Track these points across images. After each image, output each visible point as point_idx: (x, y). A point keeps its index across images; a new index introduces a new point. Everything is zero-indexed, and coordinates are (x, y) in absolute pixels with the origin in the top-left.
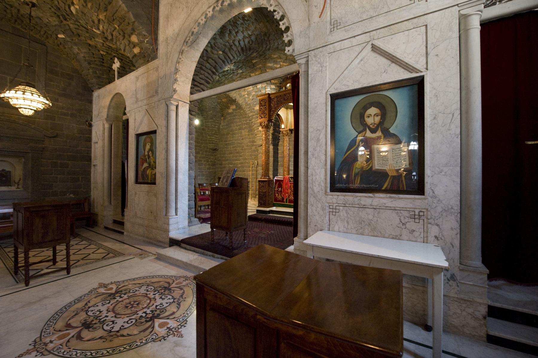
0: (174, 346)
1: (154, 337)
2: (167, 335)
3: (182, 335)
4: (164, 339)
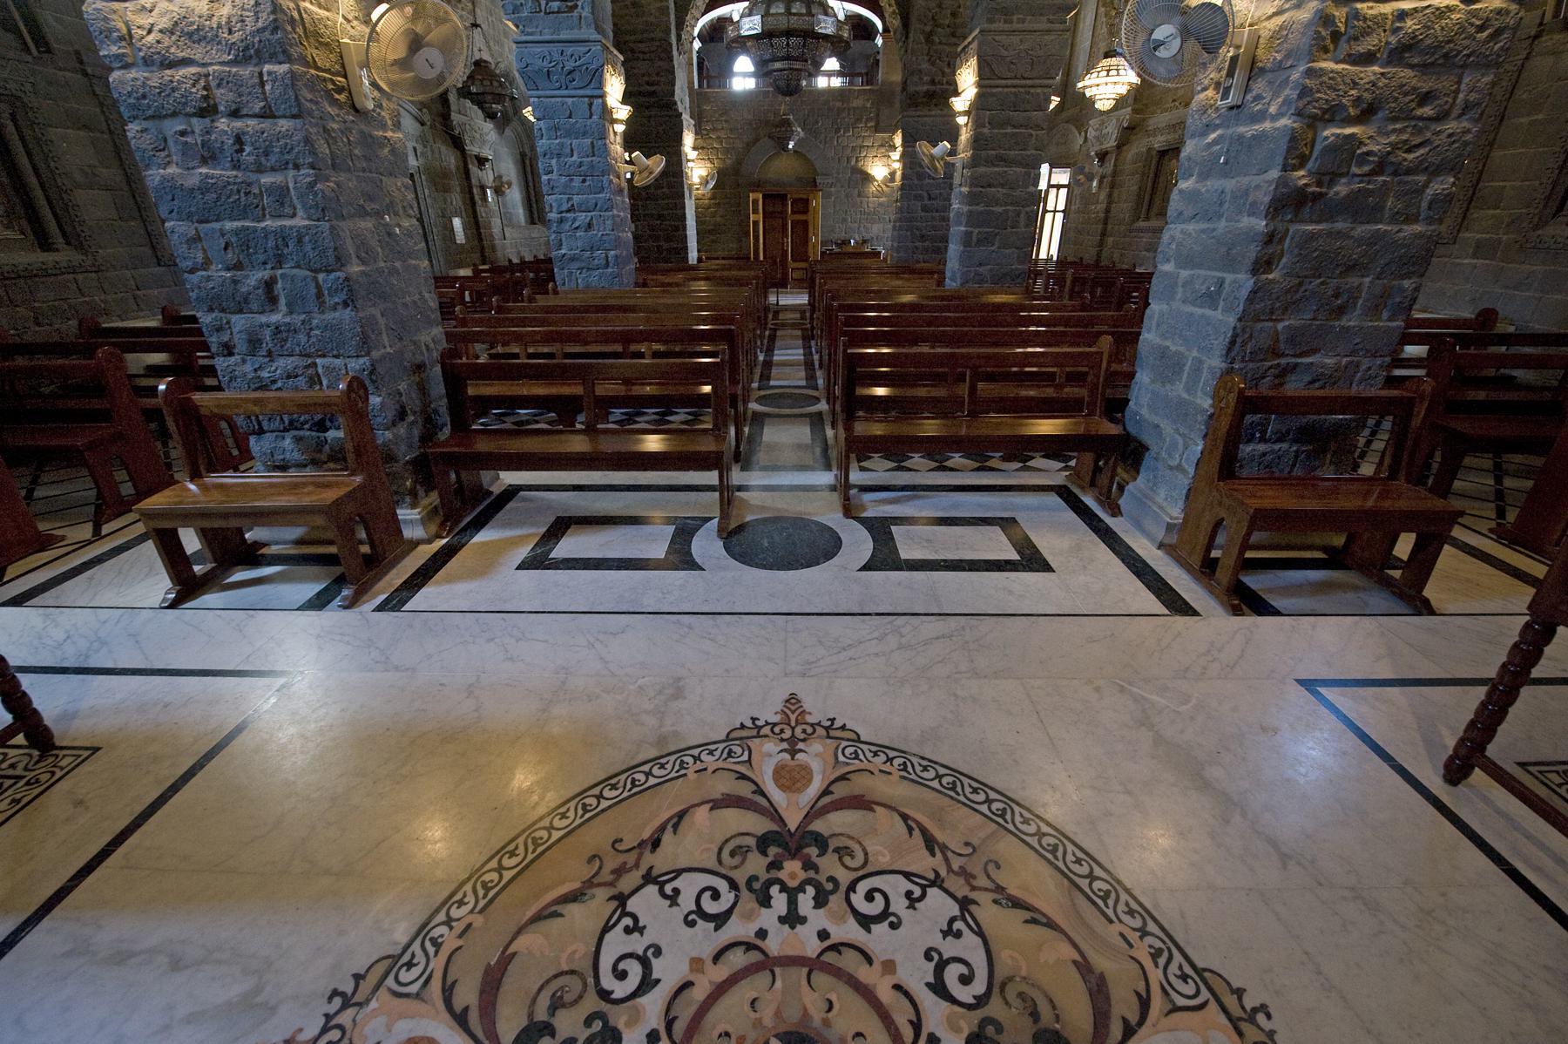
0: (258, 990)
1: (405, 976)
2: (340, 1027)
3: (787, 701)
4: (343, 994)
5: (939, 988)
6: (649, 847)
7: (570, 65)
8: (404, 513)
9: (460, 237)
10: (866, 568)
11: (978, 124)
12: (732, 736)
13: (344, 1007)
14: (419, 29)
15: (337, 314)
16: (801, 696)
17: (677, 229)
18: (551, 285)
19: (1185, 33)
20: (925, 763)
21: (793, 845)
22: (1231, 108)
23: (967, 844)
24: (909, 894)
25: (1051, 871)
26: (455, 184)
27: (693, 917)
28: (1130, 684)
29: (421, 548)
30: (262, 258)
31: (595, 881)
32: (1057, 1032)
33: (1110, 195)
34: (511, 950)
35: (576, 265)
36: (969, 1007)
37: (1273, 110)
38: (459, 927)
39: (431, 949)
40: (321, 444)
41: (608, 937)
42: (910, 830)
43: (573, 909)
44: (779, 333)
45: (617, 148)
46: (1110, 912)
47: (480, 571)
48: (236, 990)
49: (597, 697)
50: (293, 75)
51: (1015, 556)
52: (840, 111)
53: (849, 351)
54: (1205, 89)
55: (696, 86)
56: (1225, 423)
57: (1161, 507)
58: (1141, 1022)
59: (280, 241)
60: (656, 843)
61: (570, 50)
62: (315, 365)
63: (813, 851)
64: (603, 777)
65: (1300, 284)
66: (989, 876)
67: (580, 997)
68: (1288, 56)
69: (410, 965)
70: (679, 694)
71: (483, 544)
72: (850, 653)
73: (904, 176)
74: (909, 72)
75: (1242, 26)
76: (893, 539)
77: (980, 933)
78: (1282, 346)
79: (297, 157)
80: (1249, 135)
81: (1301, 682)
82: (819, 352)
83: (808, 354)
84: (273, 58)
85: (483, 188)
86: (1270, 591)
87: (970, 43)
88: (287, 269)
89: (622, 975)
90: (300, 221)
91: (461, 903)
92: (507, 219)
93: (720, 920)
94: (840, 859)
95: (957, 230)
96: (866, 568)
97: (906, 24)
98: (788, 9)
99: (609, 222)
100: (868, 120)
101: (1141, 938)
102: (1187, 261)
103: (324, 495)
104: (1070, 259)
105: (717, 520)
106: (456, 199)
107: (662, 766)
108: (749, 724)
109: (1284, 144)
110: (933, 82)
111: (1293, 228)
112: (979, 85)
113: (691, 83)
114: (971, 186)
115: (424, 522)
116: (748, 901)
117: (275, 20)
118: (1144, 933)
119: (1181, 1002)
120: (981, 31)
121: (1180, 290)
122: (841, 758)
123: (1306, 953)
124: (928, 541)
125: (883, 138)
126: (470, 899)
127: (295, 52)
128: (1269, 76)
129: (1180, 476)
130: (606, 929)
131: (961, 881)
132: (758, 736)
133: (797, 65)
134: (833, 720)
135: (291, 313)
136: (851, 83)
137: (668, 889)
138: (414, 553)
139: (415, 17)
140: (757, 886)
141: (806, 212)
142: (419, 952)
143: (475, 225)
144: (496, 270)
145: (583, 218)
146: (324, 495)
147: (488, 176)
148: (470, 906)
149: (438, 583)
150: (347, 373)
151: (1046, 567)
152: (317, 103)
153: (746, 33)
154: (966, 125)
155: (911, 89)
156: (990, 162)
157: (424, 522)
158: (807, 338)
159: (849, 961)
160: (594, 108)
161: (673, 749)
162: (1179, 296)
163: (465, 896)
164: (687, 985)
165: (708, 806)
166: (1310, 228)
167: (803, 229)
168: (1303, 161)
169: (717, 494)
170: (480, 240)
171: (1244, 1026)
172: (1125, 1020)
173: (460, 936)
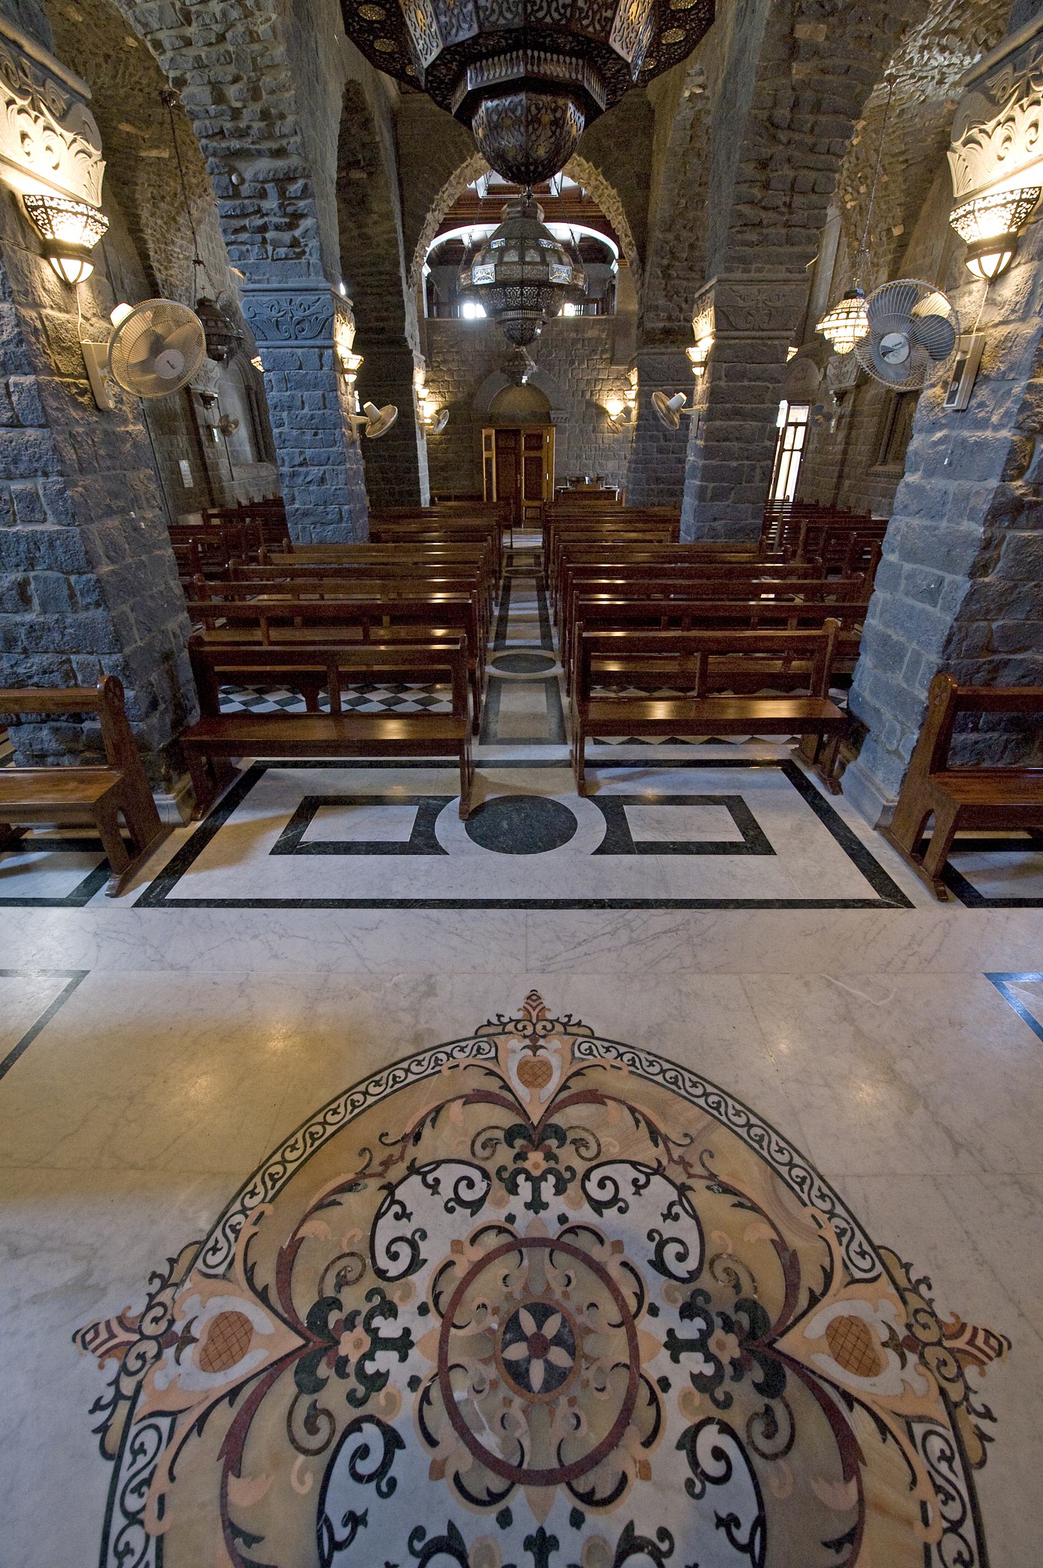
0: (89, 1273)
1: (212, 1260)
2: (162, 1304)
3: (529, 998)
5: (659, 1265)
6: (412, 1141)
7: (299, 315)
8: (161, 798)
9: (188, 482)
10: (600, 851)
11: (714, 377)
12: (480, 1033)
13: (163, 1288)
14: (159, 330)
15: (90, 613)
16: (540, 993)
17: (408, 471)
18: (285, 541)
19: (913, 341)
20: (651, 1058)
21: (535, 1137)
22: (957, 411)
23: (686, 1135)
24: (635, 1182)
25: (756, 1158)
26: (182, 425)
27: (452, 1204)
28: (837, 979)
29: (178, 831)
30: (14, 561)
31: (367, 1172)
32: (755, 1302)
33: (848, 436)
34: (299, 1236)
35: (307, 521)
36: (683, 1280)
37: (995, 419)
38: (253, 1215)
39: (231, 1236)
40: (77, 735)
41: (381, 1222)
42: (637, 1122)
43: (348, 1198)
44: (514, 582)
45: (351, 399)
46: (805, 1197)
47: (234, 857)
48: (71, 1273)
49: (358, 995)
50: (40, 387)
51: (739, 838)
52: (575, 341)
53: (585, 635)
54: (933, 386)
55: (426, 315)
56: (939, 718)
57: (879, 790)
58: (823, 1294)
59: (32, 545)
60: (417, 1137)
61: (298, 299)
62: (69, 661)
63: (553, 1143)
64: (368, 1074)
65: (1016, 586)
66: (703, 1165)
67: (361, 1276)
68: (1010, 369)
69: (215, 1250)
70: (431, 991)
71: (238, 827)
72: (584, 948)
73: (640, 417)
74: (647, 307)
75: (968, 332)
76: (625, 819)
77: (695, 1217)
78: (996, 644)
79: (46, 465)
80: (972, 440)
81: (988, 975)
82: (554, 605)
83: (543, 608)
84: (18, 369)
85: (209, 428)
86: (977, 874)
87: (707, 291)
88: (38, 572)
89: (394, 1257)
90: (51, 526)
91: (253, 1194)
92: (235, 460)
93: (475, 1206)
94: (577, 1150)
95: (692, 483)
96: (600, 851)
97: (642, 259)
98: (522, 257)
99: (342, 477)
100: (603, 352)
101: (829, 1219)
102: (909, 555)
103: (89, 793)
104: (806, 501)
105: (458, 800)
106: (182, 441)
107: (419, 1063)
108: (495, 1020)
109: (1003, 455)
110: (670, 318)
111: (1010, 534)
112: (716, 336)
113: (420, 311)
114: (706, 440)
115: (179, 807)
116: (499, 1189)
117: (20, 333)
118: (832, 1214)
119: (858, 1275)
120: (719, 281)
121: (903, 582)
122: (577, 1054)
123: (967, 1232)
124: (658, 822)
125: (619, 371)
126: (260, 1189)
127: (38, 363)
128: (993, 385)
129: (897, 761)
130: (379, 1215)
131: (680, 1169)
132: (504, 1033)
133: (531, 314)
134: (570, 1016)
135: (45, 612)
136: (586, 312)
137: (430, 1179)
138: (171, 838)
139: (155, 320)
140: (506, 1175)
141: (539, 448)
142: (221, 1239)
143: (203, 467)
144: (226, 515)
145: (315, 471)
146: (89, 793)
147: (213, 415)
148: (261, 1196)
149: (198, 869)
150: (102, 673)
151: (769, 851)
152: (62, 410)
153: (480, 282)
154: (703, 376)
155: (649, 325)
156: (727, 416)
157: (179, 807)
158: (541, 589)
159: (584, 1242)
160: (324, 359)
161: (427, 1046)
162: (902, 588)
163: (255, 1187)
164: (450, 1264)
165: (461, 1101)
166: (1026, 534)
167: (536, 465)
168: (1021, 471)
169: (458, 770)
170: (209, 482)
171: (909, 1296)
172: (811, 1291)
173: (255, 1224)
